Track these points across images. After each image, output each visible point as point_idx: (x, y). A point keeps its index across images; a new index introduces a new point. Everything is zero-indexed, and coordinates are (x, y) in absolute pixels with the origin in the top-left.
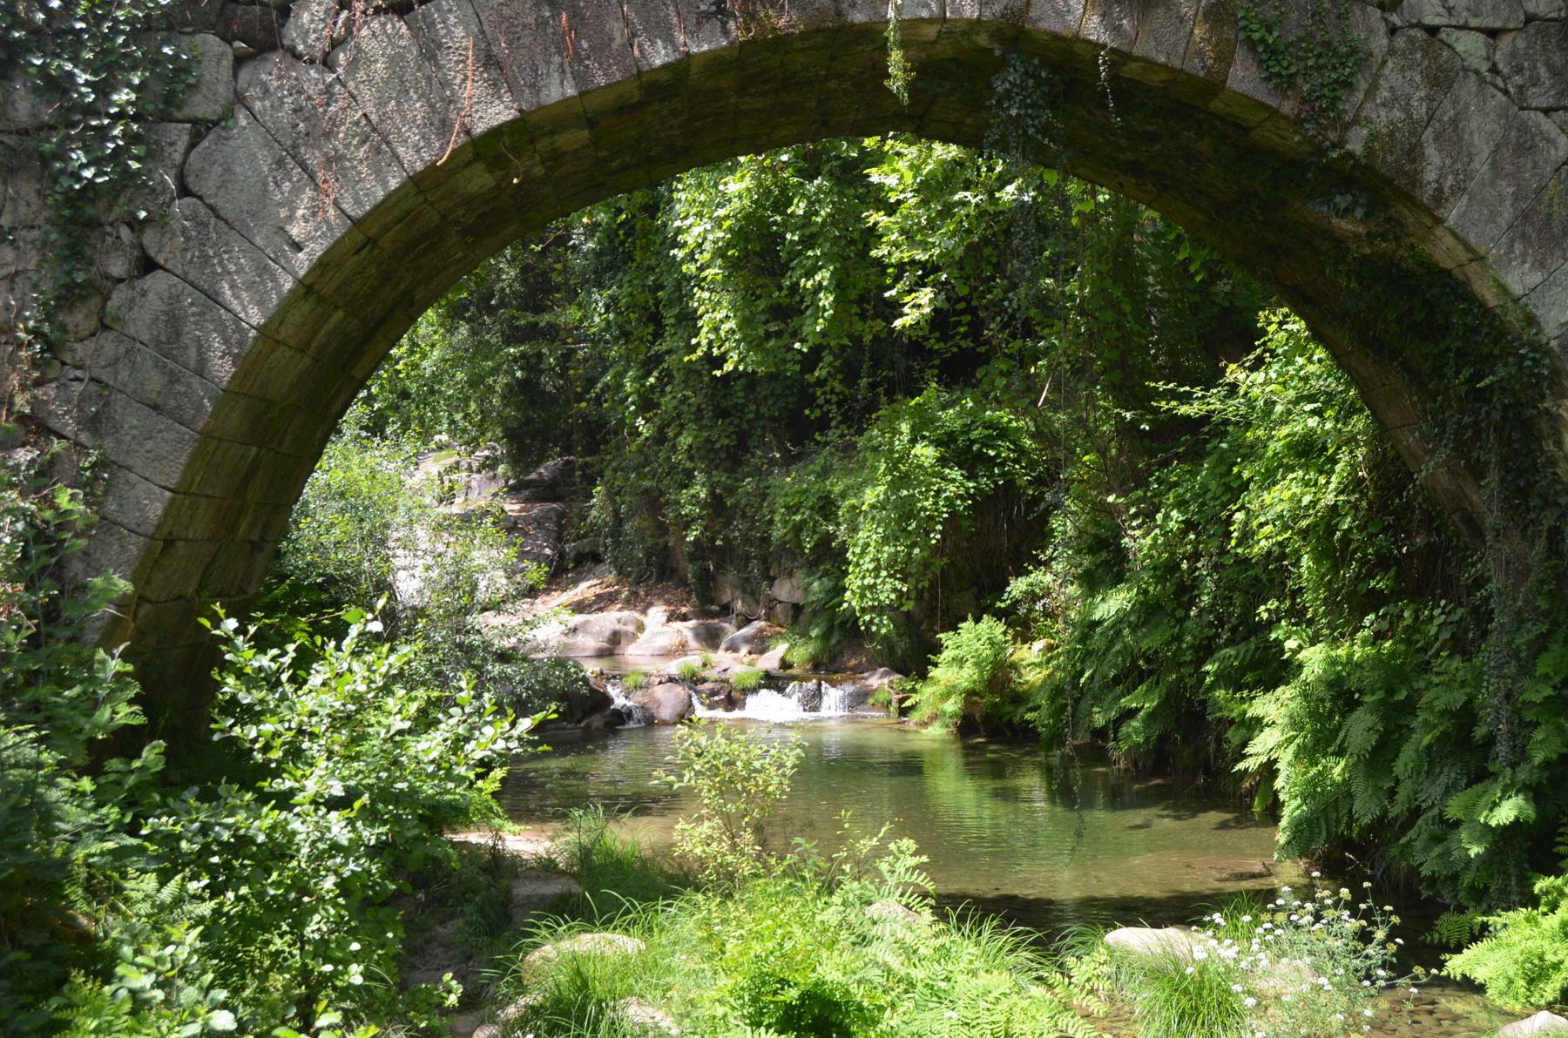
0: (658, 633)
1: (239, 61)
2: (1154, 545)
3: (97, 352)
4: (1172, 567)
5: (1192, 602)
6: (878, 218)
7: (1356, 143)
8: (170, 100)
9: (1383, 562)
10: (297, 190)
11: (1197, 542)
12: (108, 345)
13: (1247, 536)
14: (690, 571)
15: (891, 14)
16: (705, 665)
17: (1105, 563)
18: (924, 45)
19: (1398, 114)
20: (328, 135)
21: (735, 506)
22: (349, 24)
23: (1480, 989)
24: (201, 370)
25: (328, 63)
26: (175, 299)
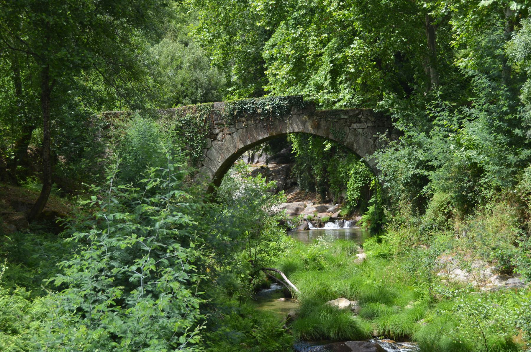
0: (310, 208)
7: (345, 144)
8: (205, 147)
16: (314, 216)
25: (222, 141)
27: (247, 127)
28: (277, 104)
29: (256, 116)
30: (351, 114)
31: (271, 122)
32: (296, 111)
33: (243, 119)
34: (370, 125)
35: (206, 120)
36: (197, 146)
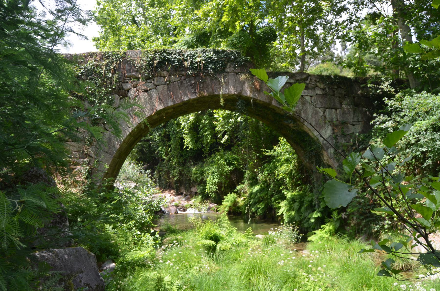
1: (121, 99)
2: (263, 178)
4: (266, 181)
5: (269, 188)
6: (215, 123)
9: (300, 179)
11: (270, 178)
13: (278, 175)
14: (174, 186)
15: (221, 93)
17: (255, 182)
18: (225, 97)
19: (297, 108)
21: (184, 174)
22: (138, 93)
23: (313, 242)
24: (114, 147)
26: (110, 135)
27: (169, 84)
28: (210, 58)
29: (182, 71)
30: (298, 78)
31: (202, 79)
32: (232, 69)
33: (165, 73)
34: (319, 92)
35: (115, 71)
36: (100, 103)
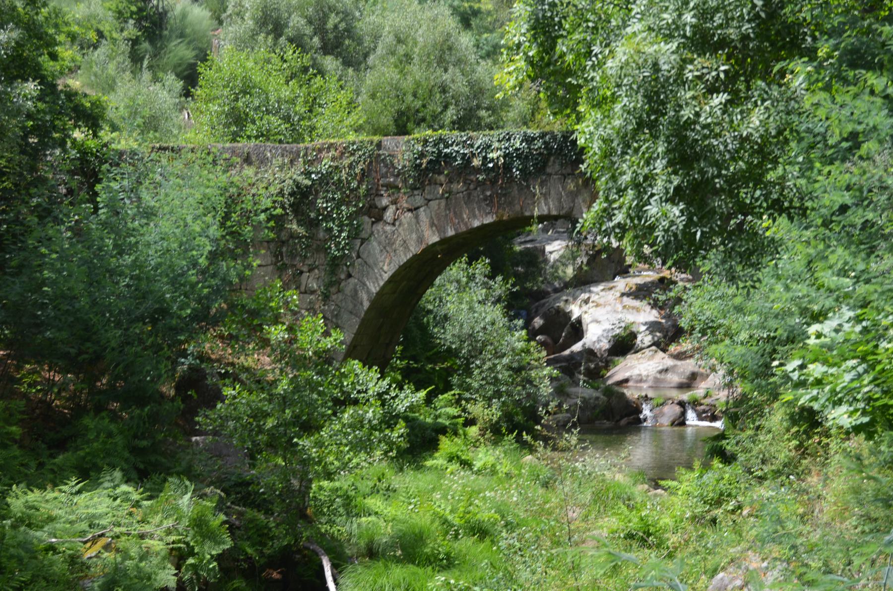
3: (337, 298)
10: (385, 258)
12: (340, 296)
20: (393, 244)
25: (394, 224)
